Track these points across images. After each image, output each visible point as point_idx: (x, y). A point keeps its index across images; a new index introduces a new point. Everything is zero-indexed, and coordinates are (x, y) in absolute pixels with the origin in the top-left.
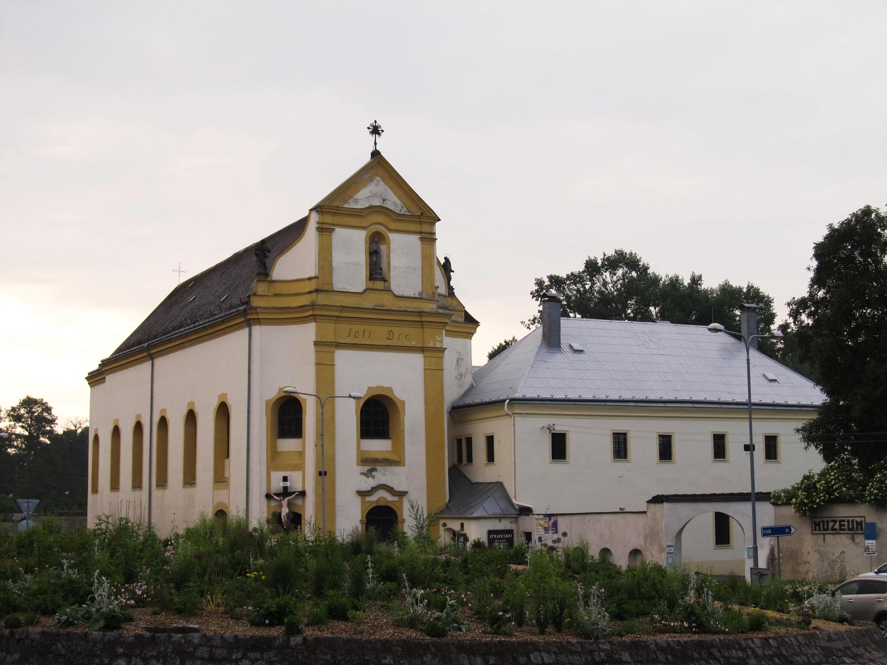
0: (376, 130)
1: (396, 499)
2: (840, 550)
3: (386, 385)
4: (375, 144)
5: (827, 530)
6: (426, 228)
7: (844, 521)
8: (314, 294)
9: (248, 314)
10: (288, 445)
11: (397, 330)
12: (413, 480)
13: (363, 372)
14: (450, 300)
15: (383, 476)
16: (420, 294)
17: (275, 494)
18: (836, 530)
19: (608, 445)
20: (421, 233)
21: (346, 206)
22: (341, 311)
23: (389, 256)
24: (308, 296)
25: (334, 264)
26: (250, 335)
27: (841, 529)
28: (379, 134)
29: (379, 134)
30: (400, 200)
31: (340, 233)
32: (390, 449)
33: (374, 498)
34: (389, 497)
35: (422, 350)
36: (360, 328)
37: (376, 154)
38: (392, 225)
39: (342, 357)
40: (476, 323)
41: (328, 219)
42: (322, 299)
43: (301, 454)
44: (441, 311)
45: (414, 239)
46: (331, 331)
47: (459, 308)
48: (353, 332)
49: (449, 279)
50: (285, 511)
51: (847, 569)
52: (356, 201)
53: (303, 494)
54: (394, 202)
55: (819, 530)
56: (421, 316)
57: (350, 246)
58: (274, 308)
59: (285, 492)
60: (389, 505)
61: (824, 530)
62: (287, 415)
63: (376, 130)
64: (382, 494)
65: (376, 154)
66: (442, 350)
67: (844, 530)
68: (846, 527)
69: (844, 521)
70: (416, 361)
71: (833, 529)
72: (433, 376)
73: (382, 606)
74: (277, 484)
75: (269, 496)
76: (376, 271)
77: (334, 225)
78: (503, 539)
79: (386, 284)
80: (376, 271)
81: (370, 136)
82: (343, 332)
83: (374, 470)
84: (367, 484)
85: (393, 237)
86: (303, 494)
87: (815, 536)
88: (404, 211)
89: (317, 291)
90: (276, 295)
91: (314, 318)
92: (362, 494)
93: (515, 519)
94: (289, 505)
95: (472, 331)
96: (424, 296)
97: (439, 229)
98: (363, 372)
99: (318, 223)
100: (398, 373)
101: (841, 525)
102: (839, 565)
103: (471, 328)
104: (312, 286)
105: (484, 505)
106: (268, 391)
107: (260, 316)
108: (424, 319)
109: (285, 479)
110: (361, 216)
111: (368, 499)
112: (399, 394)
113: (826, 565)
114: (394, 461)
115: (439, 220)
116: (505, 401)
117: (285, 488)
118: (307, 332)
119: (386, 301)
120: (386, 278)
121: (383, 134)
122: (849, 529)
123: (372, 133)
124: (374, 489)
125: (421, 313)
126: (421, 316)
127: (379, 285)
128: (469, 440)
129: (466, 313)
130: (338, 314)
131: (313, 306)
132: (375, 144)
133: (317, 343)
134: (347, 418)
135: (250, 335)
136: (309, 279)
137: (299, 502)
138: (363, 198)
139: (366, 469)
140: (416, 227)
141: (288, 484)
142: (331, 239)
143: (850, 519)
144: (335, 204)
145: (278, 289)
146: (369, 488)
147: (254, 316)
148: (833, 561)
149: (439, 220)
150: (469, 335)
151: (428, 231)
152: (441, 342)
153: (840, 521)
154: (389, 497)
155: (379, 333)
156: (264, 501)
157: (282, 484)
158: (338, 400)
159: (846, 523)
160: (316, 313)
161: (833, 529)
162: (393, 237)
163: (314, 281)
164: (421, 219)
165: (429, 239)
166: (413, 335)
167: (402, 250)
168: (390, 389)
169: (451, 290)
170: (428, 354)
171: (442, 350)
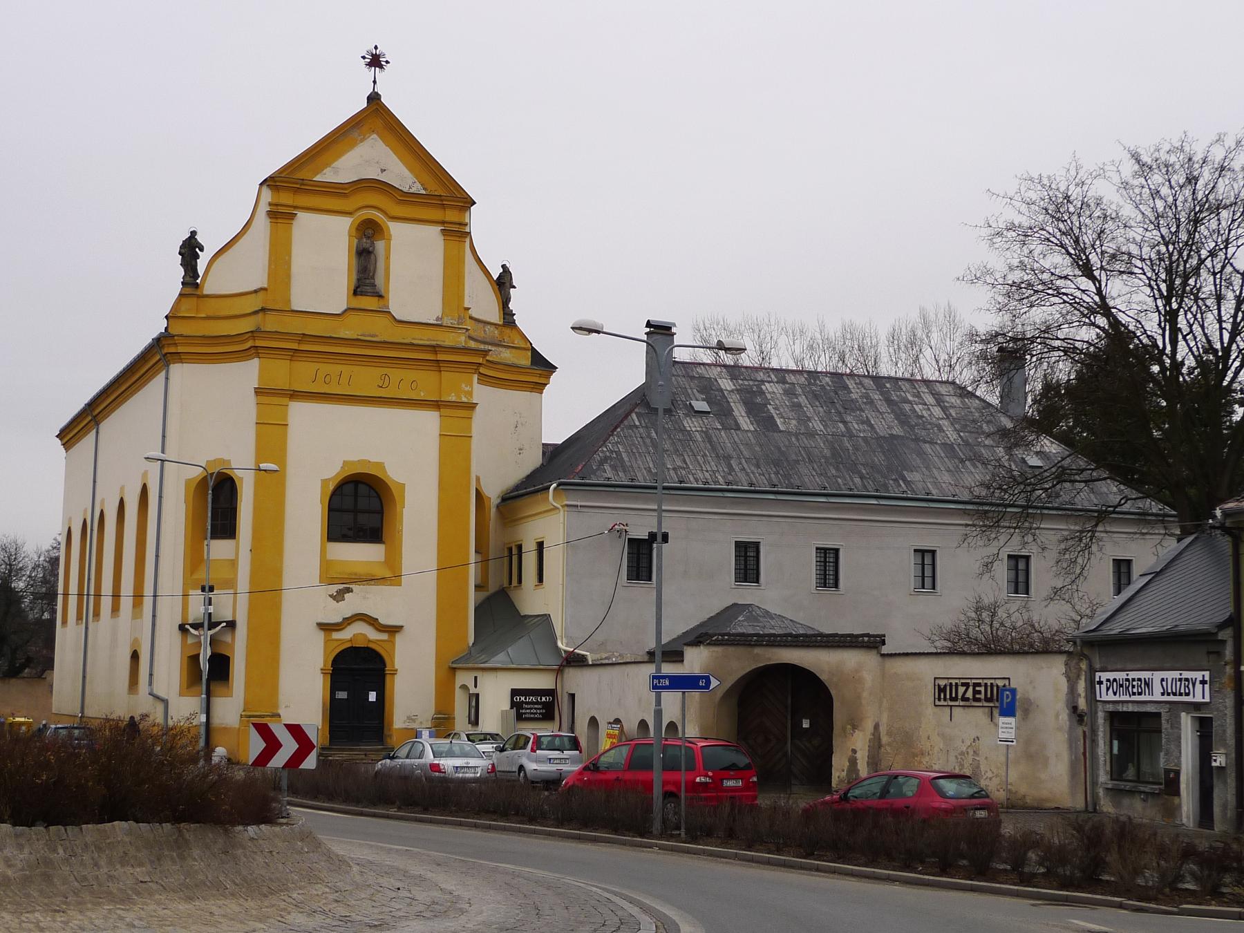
0: (375, 61)
1: (384, 636)
2: (974, 734)
3: (374, 459)
4: (375, 82)
5: (955, 699)
6: (451, 215)
7: (979, 685)
8: (261, 315)
9: (163, 346)
10: (220, 549)
11: (396, 374)
12: (411, 603)
13: (330, 439)
14: (507, 331)
15: (356, 602)
16: (438, 319)
18: (968, 700)
19: (910, 563)
20: (443, 223)
21: (318, 178)
22: (300, 342)
23: (388, 258)
24: (253, 318)
25: (295, 268)
26: (167, 378)
27: (976, 700)
28: (381, 67)
29: (381, 67)
30: (410, 170)
31: (304, 220)
32: (383, 559)
33: (347, 634)
34: (373, 635)
35: (437, 405)
36: (333, 369)
37: (374, 98)
39: (300, 414)
40: (553, 368)
41: (286, 198)
42: (271, 323)
43: (233, 563)
44: (473, 344)
45: (432, 233)
46: (282, 373)
47: (518, 342)
48: (321, 375)
49: (505, 301)
51: (982, 768)
52: (336, 172)
53: (231, 625)
54: (401, 176)
55: (945, 699)
56: (436, 352)
57: (323, 242)
58: (203, 337)
60: (371, 645)
61: (952, 699)
62: (218, 501)
63: (375, 61)
64: (360, 628)
65: (374, 98)
66: (472, 407)
67: (979, 700)
68: (982, 696)
69: (979, 685)
70: (429, 421)
71: (964, 699)
72: (455, 449)
74: (197, 610)
75: (182, 628)
76: (366, 280)
77: (296, 207)
78: (537, 703)
79: (382, 302)
80: (366, 280)
81: (366, 69)
82: (305, 374)
83: (349, 590)
84: (336, 611)
85: (395, 228)
86: (231, 625)
87: (937, 709)
88: (417, 188)
89: (263, 310)
90: (208, 318)
91: (255, 351)
92: (326, 628)
93: (559, 671)
95: (542, 381)
96: (447, 321)
97: (479, 221)
98: (330, 439)
99: (270, 204)
100: (399, 444)
101: (975, 692)
102: (970, 757)
103: (541, 376)
104: (254, 304)
105: (509, 650)
107: (180, 349)
108: (441, 357)
110: (345, 195)
111: (336, 635)
112: (394, 473)
113: (952, 759)
114: (391, 575)
118: (248, 373)
119: (379, 329)
120: (383, 293)
122: (987, 700)
123: (370, 65)
124: (348, 621)
125: (435, 349)
126: (436, 352)
127: (367, 302)
128: (520, 547)
129: (534, 351)
130: (295, 346)
131: (254, 334)
132: (375, 82)
133: (259, 392)
134: (306, 512)
135: (167, 378)
136: (256, 291)
138: (347, 167)
139: (334, 589)
140: (437, 214)
141: (211, 609)
142: (290, 229)
143: (954, 682)
144: (300, 175)
145: (211, 308)
146: (339, 619)
147: (172, 350)
148: (962, 753)
150: (539, 387)
151: (456, 219)
152: (470, 394)
153: (975, 685)
154: (373, 635)
155: (365, 378)
156: (177, 635)
159: (982, 689)
160: (259, 343)
161: (964, 699)
162: (395, 228)
163: (261, 294)
164: (446, 202)
165: (457, 233)
166: (424, 383)
167: (412, 251)
168: (380, 465)
169: (508, 318)
170: (445, 411)
171: (472, 407)
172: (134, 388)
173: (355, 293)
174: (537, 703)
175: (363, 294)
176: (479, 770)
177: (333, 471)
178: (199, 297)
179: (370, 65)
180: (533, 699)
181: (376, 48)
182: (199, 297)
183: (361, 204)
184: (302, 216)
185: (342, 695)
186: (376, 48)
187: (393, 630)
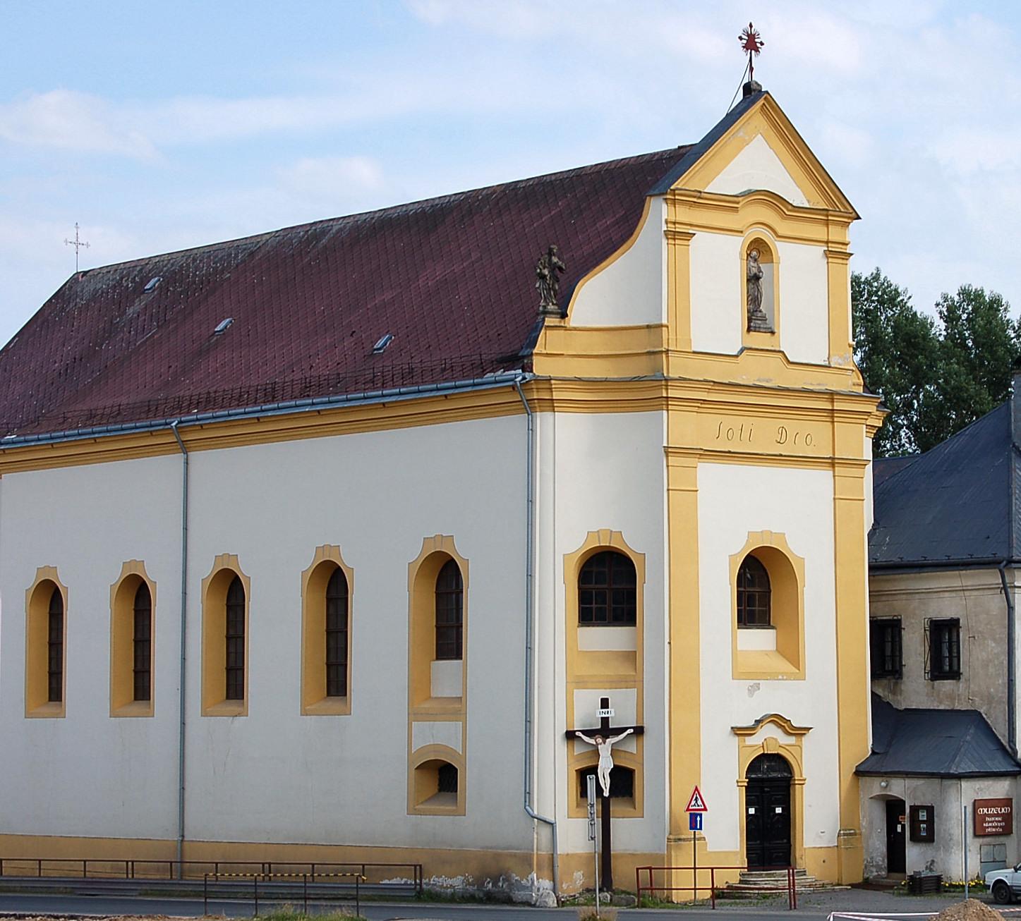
0: (751, 43)
1: (792, 740)
11: (793, 425)
17: (584, 732)
26: (187, 463)
28: (757, 50)
35: (832, 462)
36: (733, 421)
37: (751, 92)
38: (784, 227)
50: (605, 765)
59: (605, 730)
63: (751, 43)
73: (75, 359)
78: (997, 815)
94: (614, 752)
106: (565, 539)
108: (837, 406)
109: (605, 703)
111: (749, 741)
112: (794, 548)
115: (858, 218)
116: (1002, 562)
117: (605, 721)
121: (762, 49)
127: (759, 340)
135: (187, 463)
137: (632, 747)
140: (819, 232)
149: (858, 218)
156: (562, 746)
157: (601, 713)
158: (179, 458)
162: (782, 250)
172: (370, 424)
173: (749, 330)
174: (997, 815)
175: (757, 329)
176: (801, 862)
177: (740, 548)
178: (565, 328)
179: (746, 47)
180: (993, 810)
181: (751, 26)
182: (565, 328)
183: (762, 220)
184: (701, 237)
185: (752, 811)
186: (751, 26)
187: (801, 732)
